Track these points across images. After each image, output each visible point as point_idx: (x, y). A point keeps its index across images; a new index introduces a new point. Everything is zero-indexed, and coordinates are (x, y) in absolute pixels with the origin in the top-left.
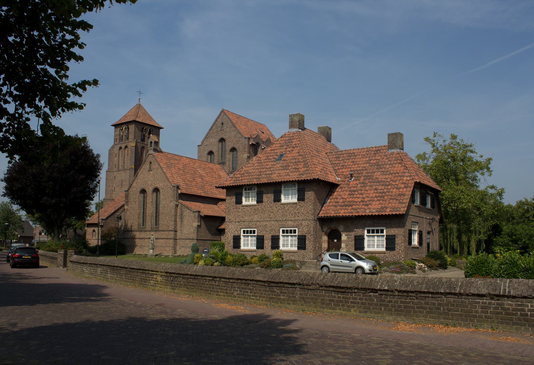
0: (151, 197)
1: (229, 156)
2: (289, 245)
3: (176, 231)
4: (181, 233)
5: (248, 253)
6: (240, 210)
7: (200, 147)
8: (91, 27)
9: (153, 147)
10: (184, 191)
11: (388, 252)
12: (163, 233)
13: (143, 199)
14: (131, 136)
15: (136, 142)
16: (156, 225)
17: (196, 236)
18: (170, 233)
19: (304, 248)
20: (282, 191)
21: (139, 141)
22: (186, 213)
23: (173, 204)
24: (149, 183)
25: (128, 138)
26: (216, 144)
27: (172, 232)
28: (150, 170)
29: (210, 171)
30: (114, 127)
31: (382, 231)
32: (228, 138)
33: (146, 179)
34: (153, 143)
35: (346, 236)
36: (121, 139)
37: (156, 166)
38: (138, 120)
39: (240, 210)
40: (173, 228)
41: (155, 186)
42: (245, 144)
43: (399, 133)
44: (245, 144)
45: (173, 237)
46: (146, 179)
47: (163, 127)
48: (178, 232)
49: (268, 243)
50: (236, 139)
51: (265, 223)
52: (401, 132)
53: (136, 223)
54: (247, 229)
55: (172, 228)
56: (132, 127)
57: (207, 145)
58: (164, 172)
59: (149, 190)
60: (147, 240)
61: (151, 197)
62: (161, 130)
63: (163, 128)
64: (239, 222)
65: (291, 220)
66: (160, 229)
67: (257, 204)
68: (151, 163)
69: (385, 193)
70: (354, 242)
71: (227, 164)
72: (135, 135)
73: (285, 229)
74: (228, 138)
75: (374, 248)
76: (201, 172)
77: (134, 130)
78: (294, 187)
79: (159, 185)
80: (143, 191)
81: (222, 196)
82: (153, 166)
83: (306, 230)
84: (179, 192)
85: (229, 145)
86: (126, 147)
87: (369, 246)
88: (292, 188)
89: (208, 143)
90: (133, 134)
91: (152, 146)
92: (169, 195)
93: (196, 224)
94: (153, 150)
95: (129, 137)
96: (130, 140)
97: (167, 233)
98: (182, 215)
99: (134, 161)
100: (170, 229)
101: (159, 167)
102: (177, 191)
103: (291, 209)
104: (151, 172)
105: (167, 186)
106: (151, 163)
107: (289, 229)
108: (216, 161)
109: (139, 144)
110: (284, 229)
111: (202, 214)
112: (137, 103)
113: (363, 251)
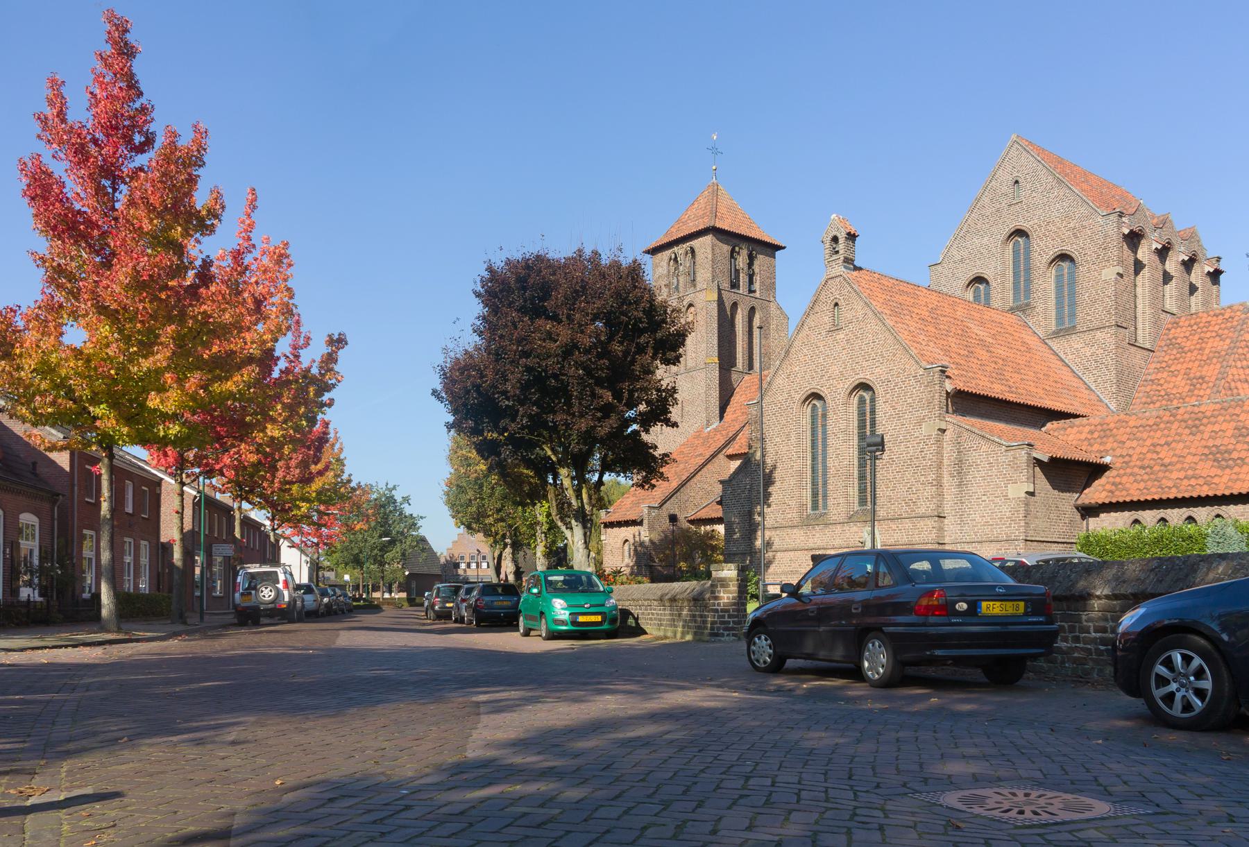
1: (1045, 283)
4: (962, 523)
7: (939, 268)
9: (841, 252)
10: (961, 386)
12: (894, 527)
13: (809, 427)
14: (703, 275)
15: (719, 290)
16: (815, 506)
17: (1022, 529)
18: (920, 523)
21: (726, 285)
23: (928, 429)
24: (835, 370)
26: (994, 250)
27: (931, 523)
28: (836, 328)
29: (999, 330)
32: (1040, 226)
33: (821, 360)
34: (841, 241)
37: (856, 312)
38: (718, 225)
40: (933, 506)
41: (859, 376)
42: (1106, 236)
44: (1106, 236)
46: (821, 360)
48: (946, 521)
50: (1072, 225)
53: (793, 503)
56: (704, 245)
57: (962, 261)
63: (784, 248)
69: (1200, 420)
71: (1040, 308)
72: (714, 271)
74: (1040, 226)
76: (979, 332)
77: (710, 256)
81: (1058, 404)
82: (846, 313)
84: (949, 386)
85: (1043, 251)
89: (965, 254)
90: (709, 266)
91: (837, 252)
92: (910, 401)
93: (1018, 490)
94: (844, 262)
95: (698, 279)
96: (699, 286)
97: (908, 524)
98: (959, 463)
99: (716, 342)
100: (922, 511)
101: (870, 313)
102: (941, 383)
104: (841, 336)
105: (904, 370)
108: (996, 302)
109: (725, 295)
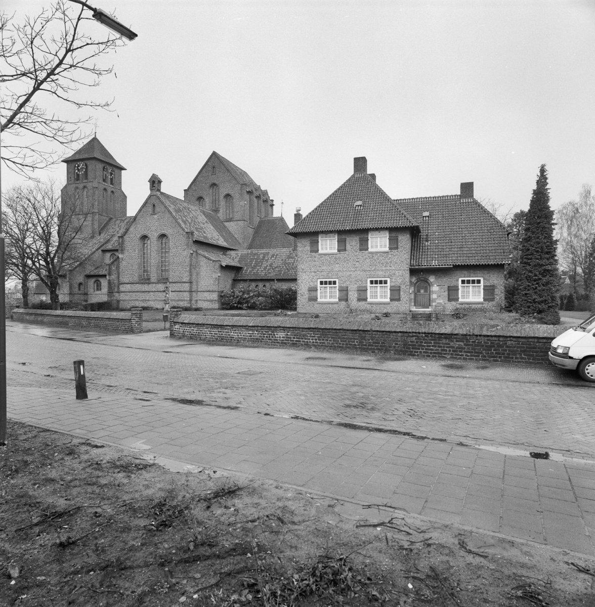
0: (153, 244)
2: (328, 297)
3: (191, 283)
5: (329, 305)
6: (316, 259)
8: (136, 35)
11: (487, 302)
19: (399, 300)
20: (369, 238)
22: (203, 262)
25: (86, 178)
27: (187, 285)
30: (65, 165)
31: (479, 282)
35: (438, 287)
36: (78, 178)
39: (316, 259)
40: (188, 279)
43: (265, 193)
45: (188, 289)
47: (125, 167)
49: (353, 296)
51: (348, 273)
52: (536, 184)
54: (381, 279)
55: (186, 279)
58: (174, 217)
59: (153, 236)
60: (152, 293)
61: (153, 244)
62: (123, 171)
64: (315, 272)
65: (382, 270)
66: (170, 280)
67: (390, 251)
68: (154, 205)
70: (447, 293)
73: (374, 279)
75: (377, 298)
78: (325, 238)
79: (168, 232)
80: (144, 237)
82: (157, 209)
83: (400, 281)
86: (85, 187)
87: (463, 297)
88: (330, 238)
103: (381, 258)
104: (156, 216)
106: (154, 205)
107: (379, 279)
110: (322, 280)
111: (224, 264)
112: (93, 136)
113: (458, 302)
